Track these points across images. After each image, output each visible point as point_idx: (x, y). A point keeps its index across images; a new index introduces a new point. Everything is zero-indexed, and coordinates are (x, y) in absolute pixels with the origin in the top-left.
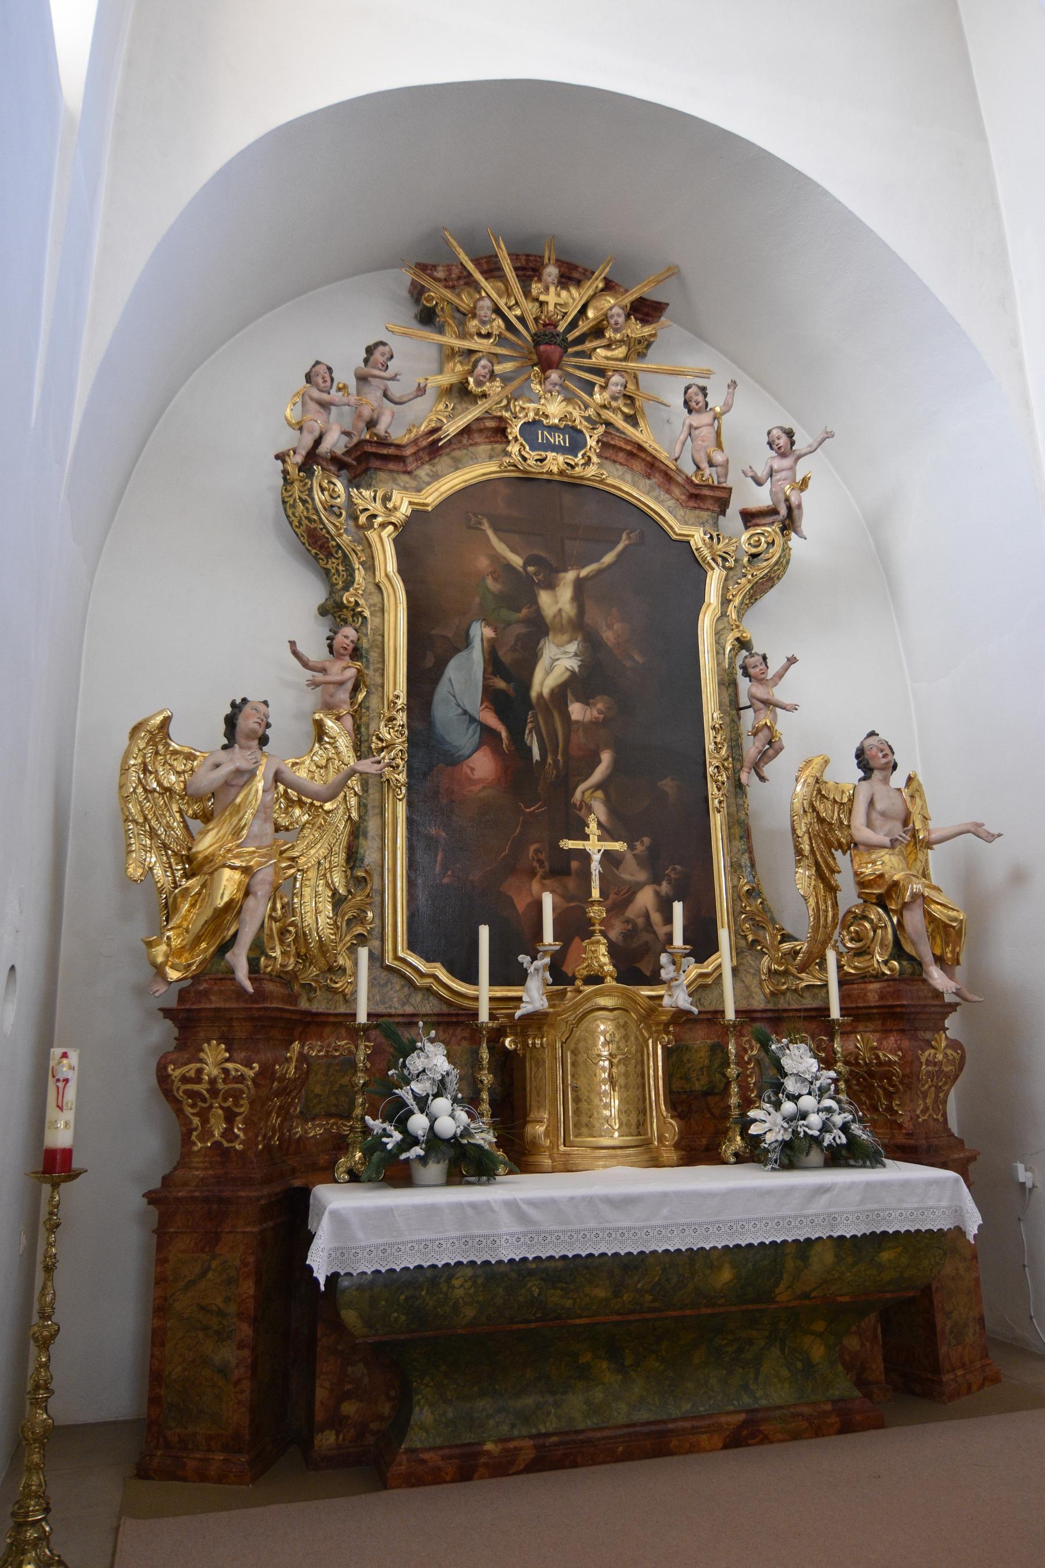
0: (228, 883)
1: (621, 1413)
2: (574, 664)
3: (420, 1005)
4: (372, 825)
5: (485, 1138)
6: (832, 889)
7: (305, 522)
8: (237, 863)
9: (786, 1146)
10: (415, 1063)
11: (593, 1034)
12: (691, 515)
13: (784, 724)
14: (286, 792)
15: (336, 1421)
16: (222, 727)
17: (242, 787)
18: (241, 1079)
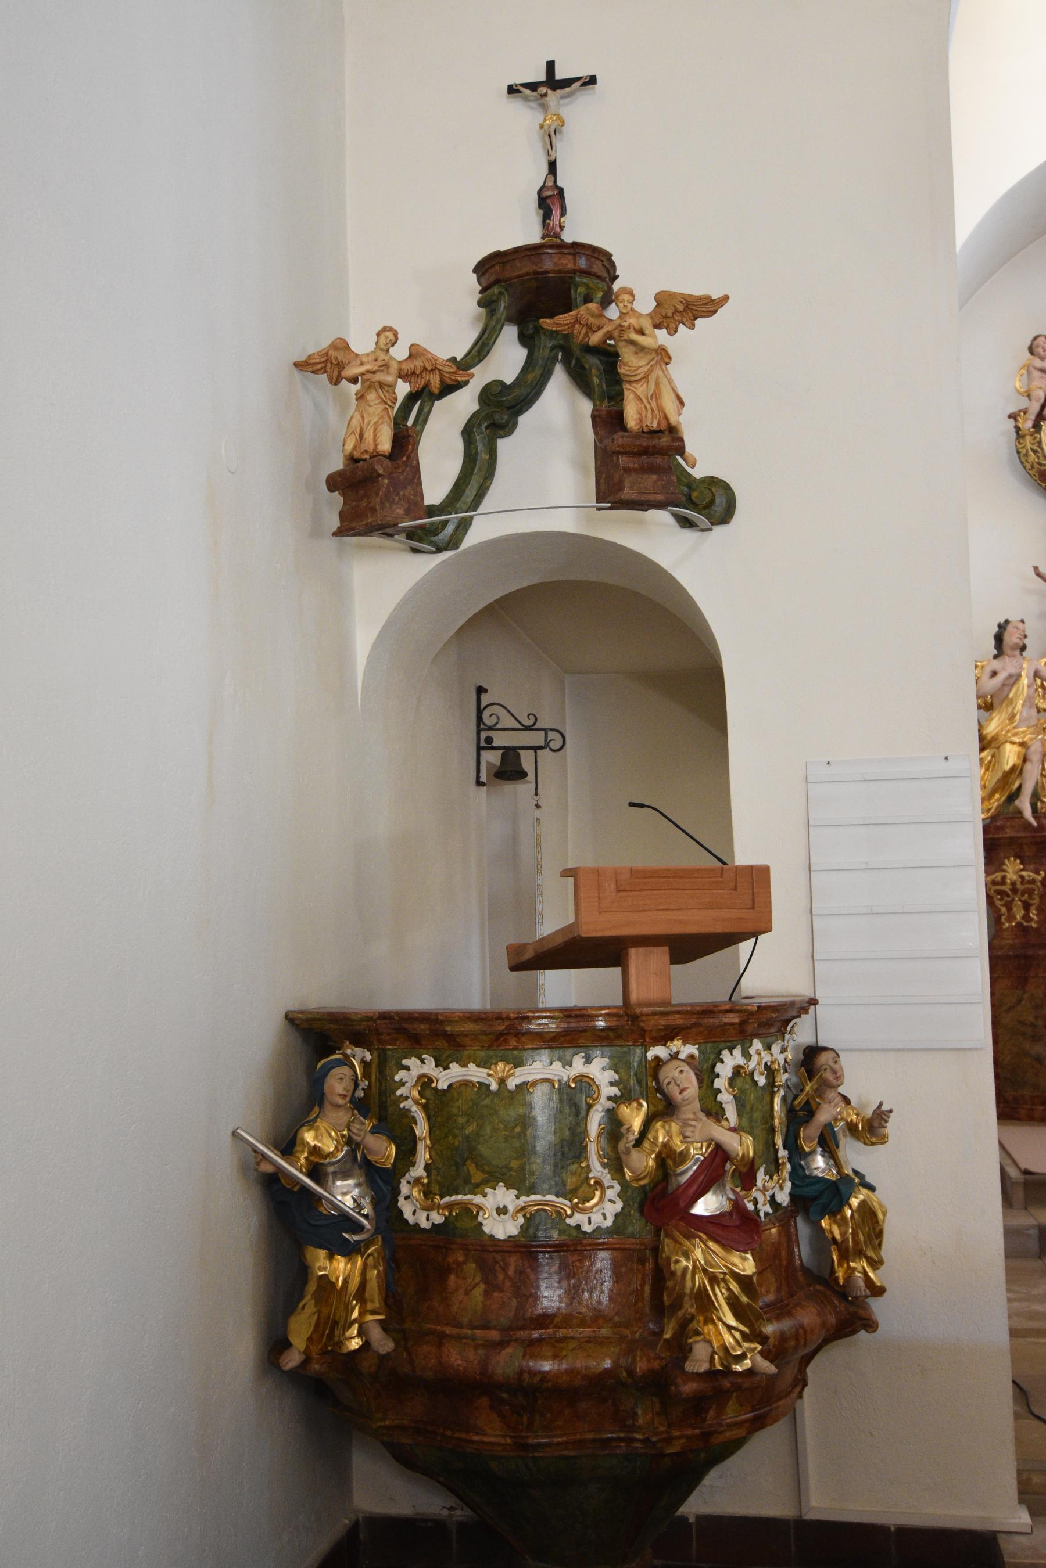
0: (1010, 755)
7: (1036, 466)
8: (1017, 740)
14: (1042, 684)
16: (993, 642)
17: (1012, 685)
18: (1033, 882)
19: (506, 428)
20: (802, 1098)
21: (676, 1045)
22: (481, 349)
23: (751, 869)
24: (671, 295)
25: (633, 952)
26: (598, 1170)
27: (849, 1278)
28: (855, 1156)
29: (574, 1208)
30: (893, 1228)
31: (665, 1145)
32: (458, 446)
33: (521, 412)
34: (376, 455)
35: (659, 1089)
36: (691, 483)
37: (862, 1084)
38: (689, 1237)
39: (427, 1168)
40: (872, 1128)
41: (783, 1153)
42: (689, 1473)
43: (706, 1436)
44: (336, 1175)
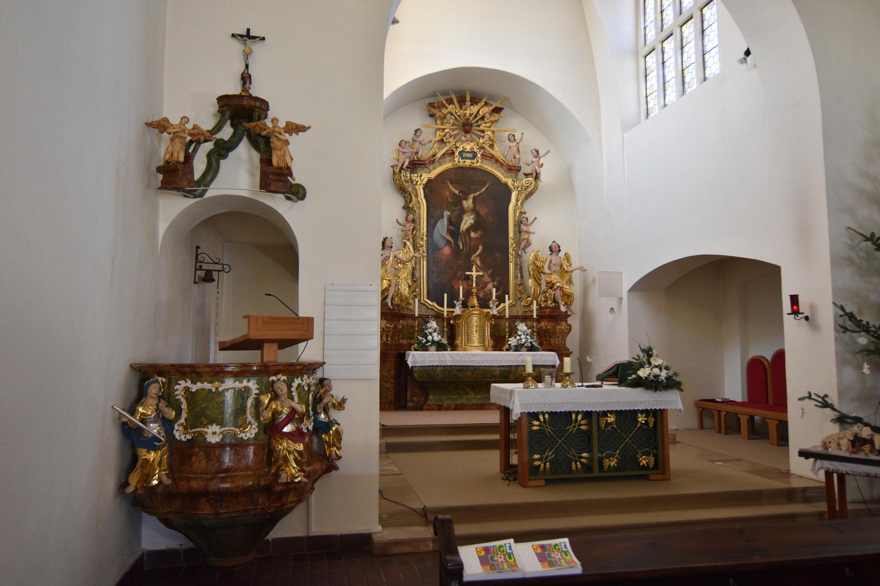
1: (474, 401)
2: (472, 221)
3: (430, 312)
4: (418, 267)
5: (445, 341)
6: (540, 285)
9: (516, 346)
10: (429, 325)
11: (472, 320)
12: (509, 175)
13: (532, 238)
15: (412, 401)
19: (225, 156)
20: (318, 395)
21: (280, 376)
22: (218, 128)
23: (308, 318)
24: (291, 123)
25: (265, 345)
26: (250, 418)
27: (330, 454)
28: (335, 415)
29: (241, 432)
30: (345, 437)
31: (275, 409)
32: (205, 160)
33: (230, 151)
34: (178, 162)
35: (273, 390)
36: (292, 185)
37: (337, 391)
38: (282, 439)
39: (186, 420)
40: (340, 405)
41: (311, 413)
42: (272, 520)
43: (282, 506)
44: (151, 422)
